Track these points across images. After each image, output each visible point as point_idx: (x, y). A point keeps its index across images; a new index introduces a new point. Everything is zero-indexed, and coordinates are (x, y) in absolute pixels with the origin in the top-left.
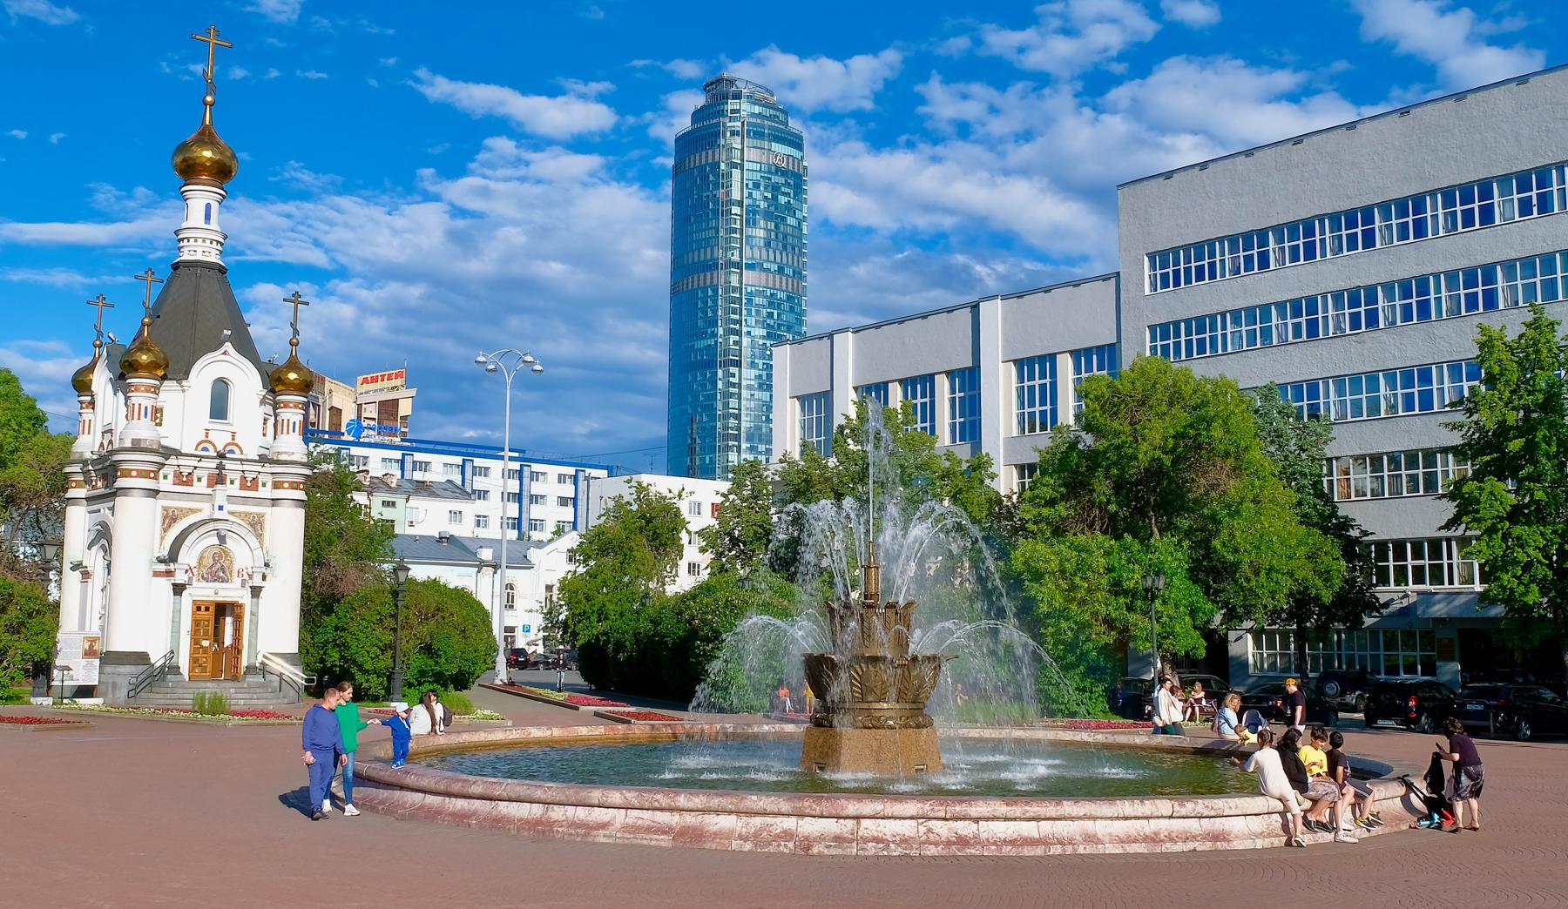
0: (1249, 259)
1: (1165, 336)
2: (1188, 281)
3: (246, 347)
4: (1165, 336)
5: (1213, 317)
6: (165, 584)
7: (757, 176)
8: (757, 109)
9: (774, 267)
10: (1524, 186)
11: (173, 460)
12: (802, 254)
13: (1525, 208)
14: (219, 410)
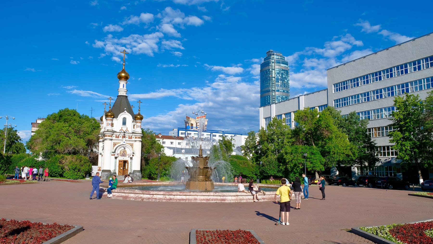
0: (354, 84)
1: (337, 102)
2: (342, 90)
3: (130, 111)
4: (337, 102)
5: (347, 97)
6: (113, 157)
7: (278, 71)
8: (278, 57)
9: (282, 91)
10: (415, 64)
11: (115, 133)
12: (288, 88)
13: (415, 69)
14: (124, 123)
